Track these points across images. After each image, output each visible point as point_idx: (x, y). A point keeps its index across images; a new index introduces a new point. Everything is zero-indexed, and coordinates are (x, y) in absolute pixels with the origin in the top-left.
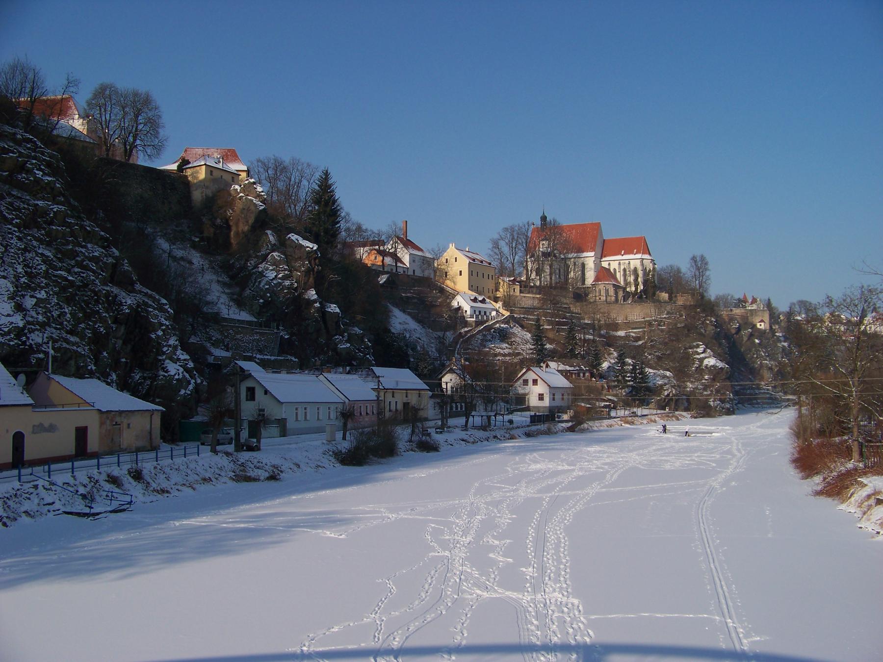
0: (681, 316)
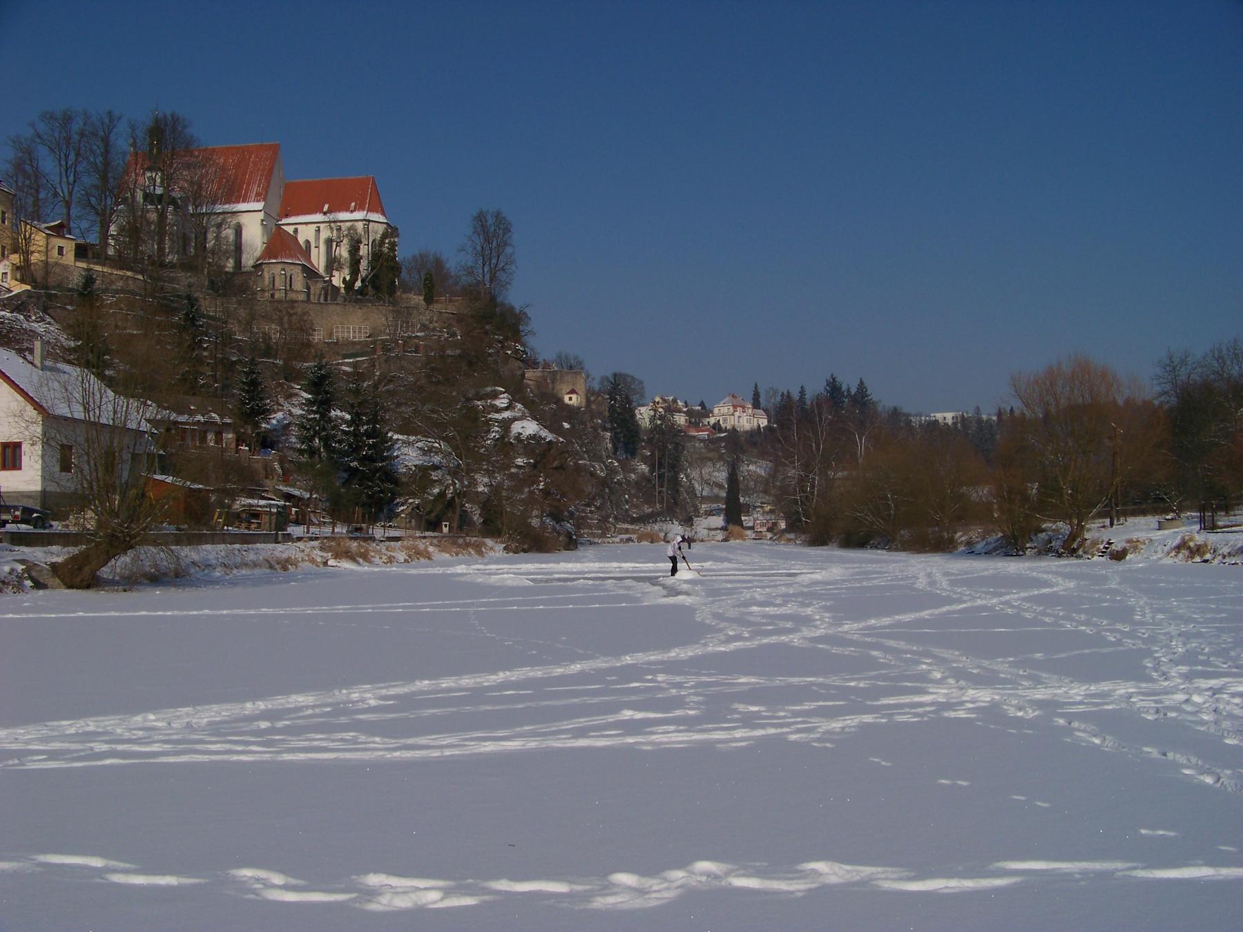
0: (454, 335)
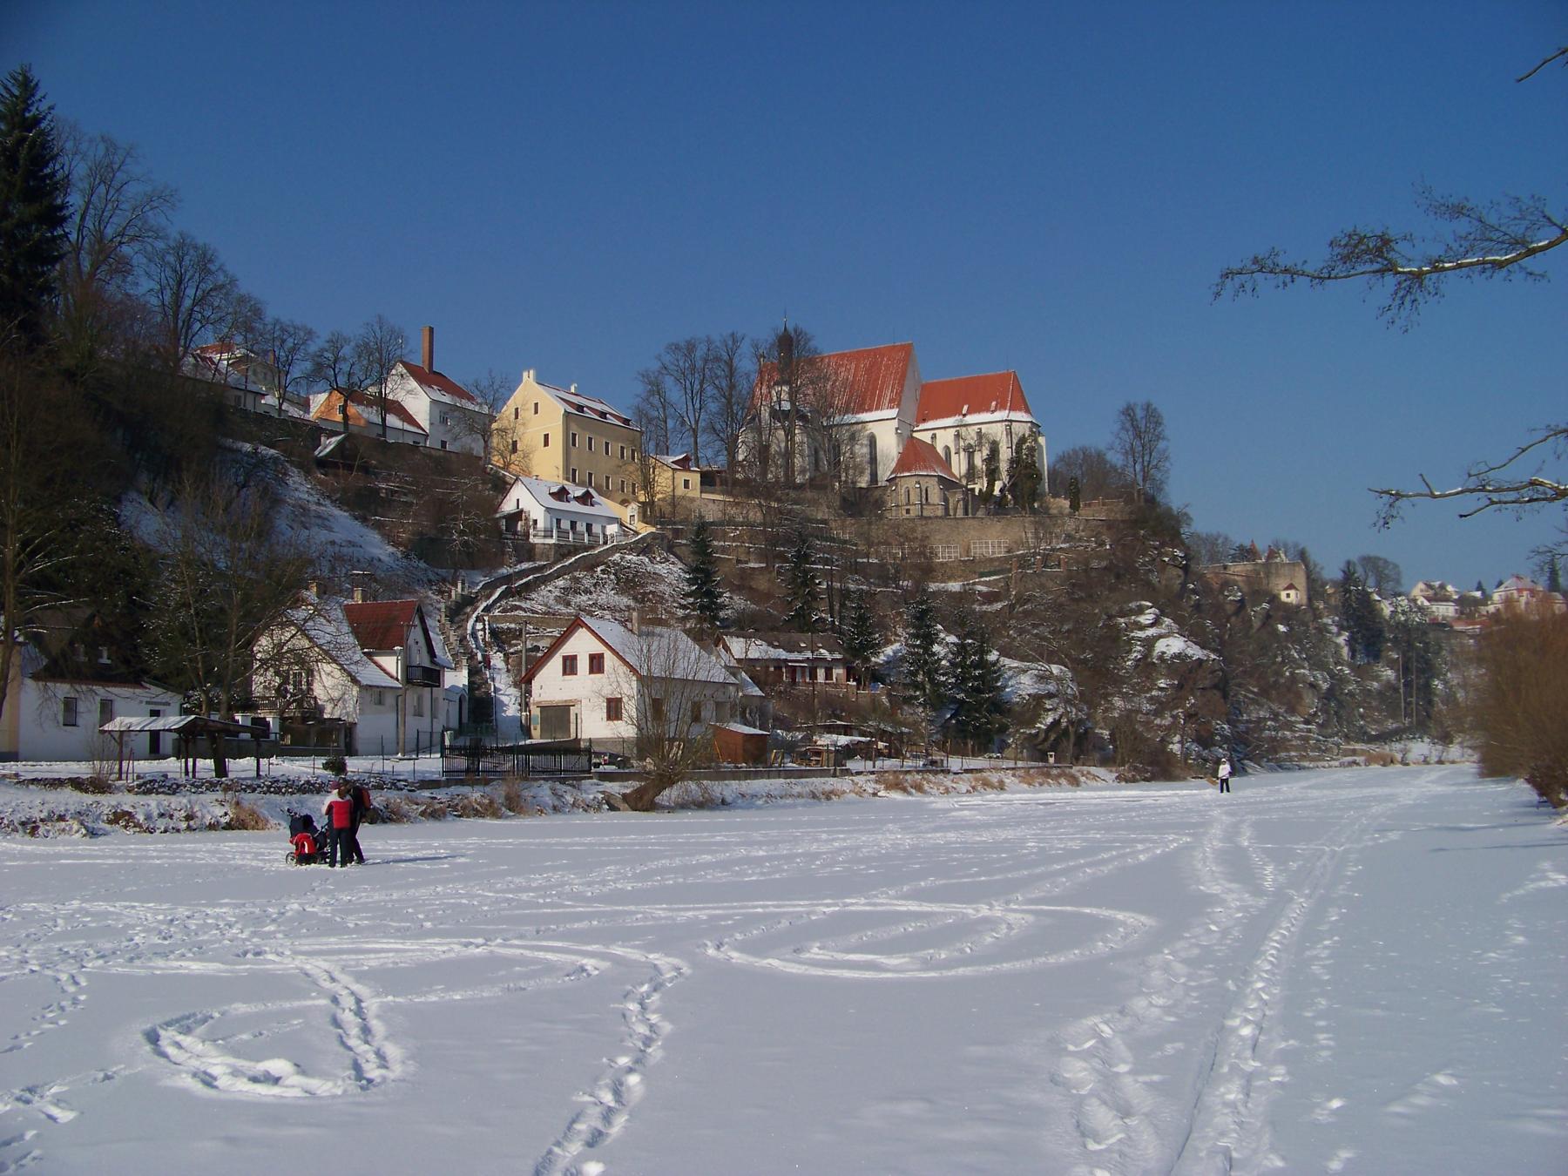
0: (1102, 544)
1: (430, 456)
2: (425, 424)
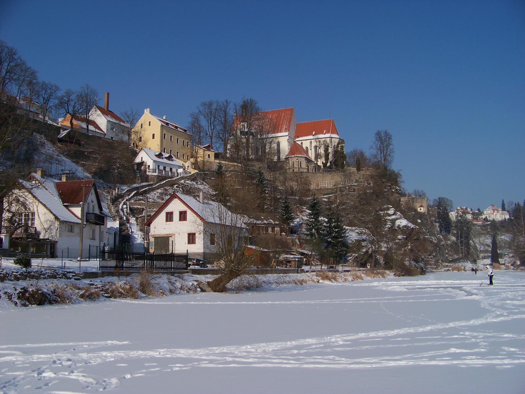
0: (369, 184)
1: (106, 142)
2: (105, 130)
